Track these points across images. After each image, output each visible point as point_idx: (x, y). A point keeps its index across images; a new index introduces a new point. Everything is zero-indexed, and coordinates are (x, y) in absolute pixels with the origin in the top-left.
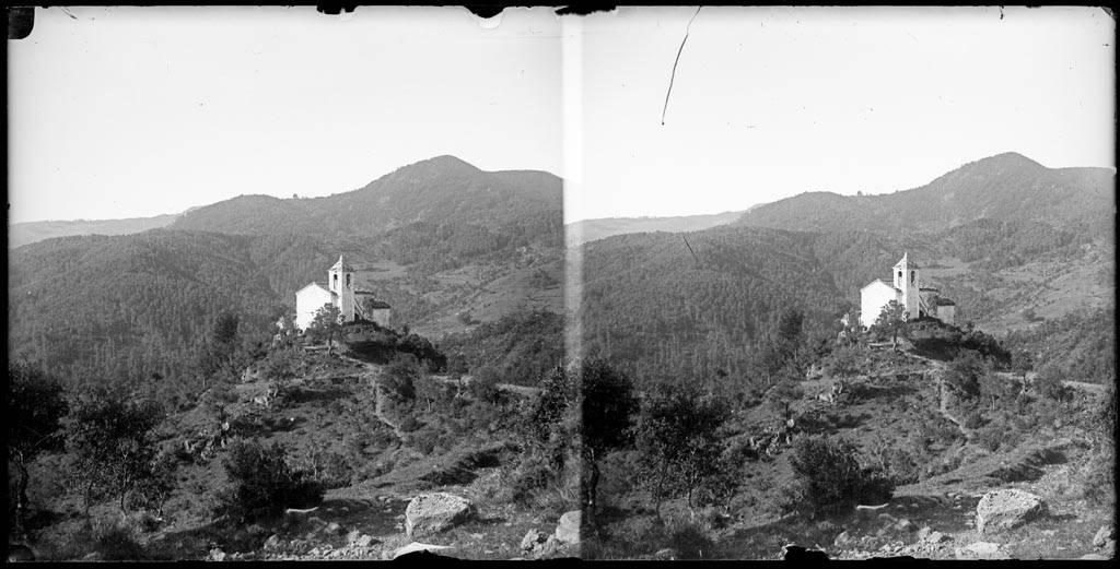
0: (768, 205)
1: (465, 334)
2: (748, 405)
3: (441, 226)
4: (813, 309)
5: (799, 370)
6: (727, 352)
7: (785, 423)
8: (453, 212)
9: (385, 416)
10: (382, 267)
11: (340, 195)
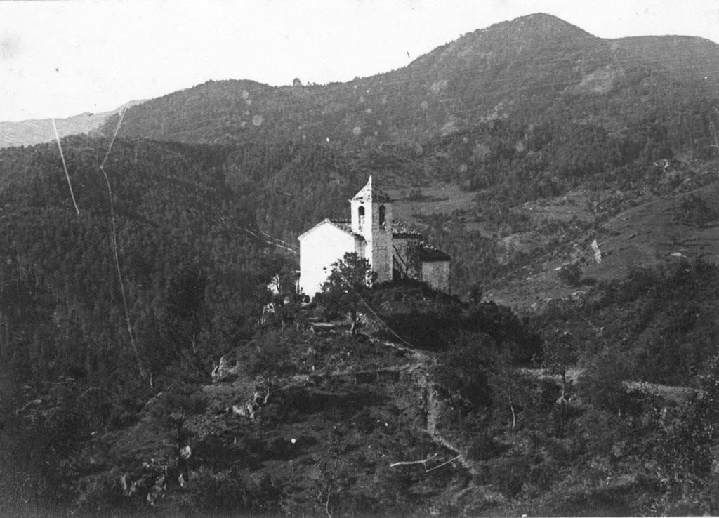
0: (148, 102)
1: (571, 301)
2: (119, 425)
3: (531, 127)
4: (223, 268)
5: (201, 367)
6: (86, 338)
7: (177, 453)
8: (551, 105)
9: (443, 435)
10: (437, 194)
11: (368, 78)
